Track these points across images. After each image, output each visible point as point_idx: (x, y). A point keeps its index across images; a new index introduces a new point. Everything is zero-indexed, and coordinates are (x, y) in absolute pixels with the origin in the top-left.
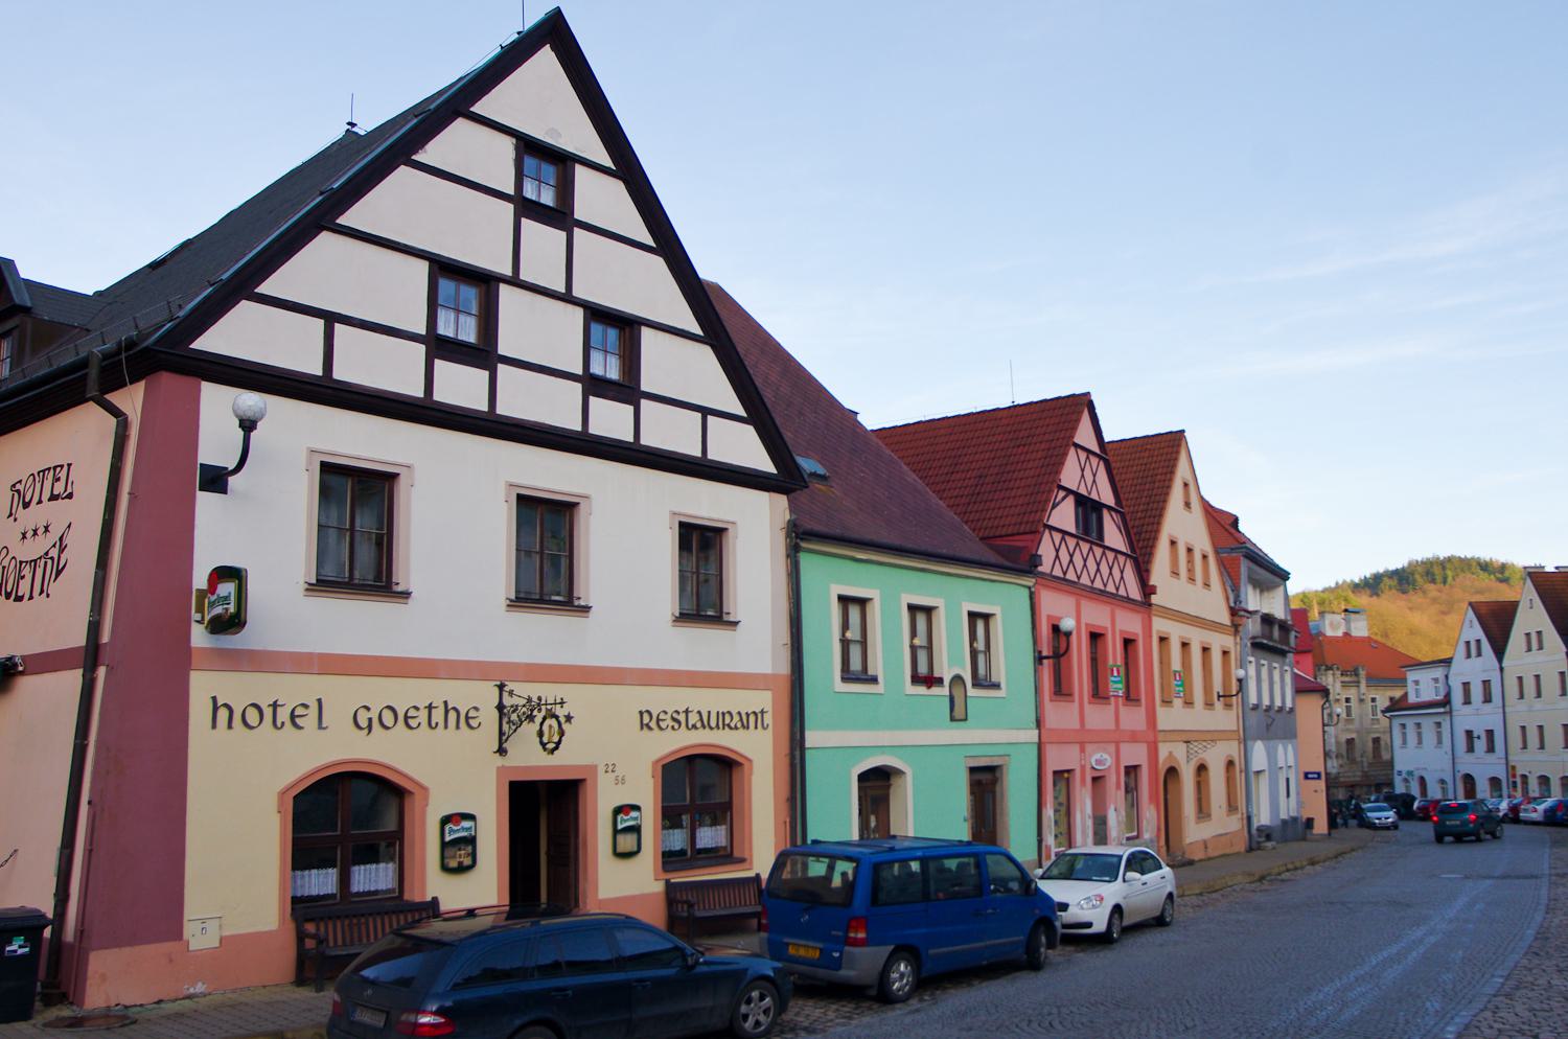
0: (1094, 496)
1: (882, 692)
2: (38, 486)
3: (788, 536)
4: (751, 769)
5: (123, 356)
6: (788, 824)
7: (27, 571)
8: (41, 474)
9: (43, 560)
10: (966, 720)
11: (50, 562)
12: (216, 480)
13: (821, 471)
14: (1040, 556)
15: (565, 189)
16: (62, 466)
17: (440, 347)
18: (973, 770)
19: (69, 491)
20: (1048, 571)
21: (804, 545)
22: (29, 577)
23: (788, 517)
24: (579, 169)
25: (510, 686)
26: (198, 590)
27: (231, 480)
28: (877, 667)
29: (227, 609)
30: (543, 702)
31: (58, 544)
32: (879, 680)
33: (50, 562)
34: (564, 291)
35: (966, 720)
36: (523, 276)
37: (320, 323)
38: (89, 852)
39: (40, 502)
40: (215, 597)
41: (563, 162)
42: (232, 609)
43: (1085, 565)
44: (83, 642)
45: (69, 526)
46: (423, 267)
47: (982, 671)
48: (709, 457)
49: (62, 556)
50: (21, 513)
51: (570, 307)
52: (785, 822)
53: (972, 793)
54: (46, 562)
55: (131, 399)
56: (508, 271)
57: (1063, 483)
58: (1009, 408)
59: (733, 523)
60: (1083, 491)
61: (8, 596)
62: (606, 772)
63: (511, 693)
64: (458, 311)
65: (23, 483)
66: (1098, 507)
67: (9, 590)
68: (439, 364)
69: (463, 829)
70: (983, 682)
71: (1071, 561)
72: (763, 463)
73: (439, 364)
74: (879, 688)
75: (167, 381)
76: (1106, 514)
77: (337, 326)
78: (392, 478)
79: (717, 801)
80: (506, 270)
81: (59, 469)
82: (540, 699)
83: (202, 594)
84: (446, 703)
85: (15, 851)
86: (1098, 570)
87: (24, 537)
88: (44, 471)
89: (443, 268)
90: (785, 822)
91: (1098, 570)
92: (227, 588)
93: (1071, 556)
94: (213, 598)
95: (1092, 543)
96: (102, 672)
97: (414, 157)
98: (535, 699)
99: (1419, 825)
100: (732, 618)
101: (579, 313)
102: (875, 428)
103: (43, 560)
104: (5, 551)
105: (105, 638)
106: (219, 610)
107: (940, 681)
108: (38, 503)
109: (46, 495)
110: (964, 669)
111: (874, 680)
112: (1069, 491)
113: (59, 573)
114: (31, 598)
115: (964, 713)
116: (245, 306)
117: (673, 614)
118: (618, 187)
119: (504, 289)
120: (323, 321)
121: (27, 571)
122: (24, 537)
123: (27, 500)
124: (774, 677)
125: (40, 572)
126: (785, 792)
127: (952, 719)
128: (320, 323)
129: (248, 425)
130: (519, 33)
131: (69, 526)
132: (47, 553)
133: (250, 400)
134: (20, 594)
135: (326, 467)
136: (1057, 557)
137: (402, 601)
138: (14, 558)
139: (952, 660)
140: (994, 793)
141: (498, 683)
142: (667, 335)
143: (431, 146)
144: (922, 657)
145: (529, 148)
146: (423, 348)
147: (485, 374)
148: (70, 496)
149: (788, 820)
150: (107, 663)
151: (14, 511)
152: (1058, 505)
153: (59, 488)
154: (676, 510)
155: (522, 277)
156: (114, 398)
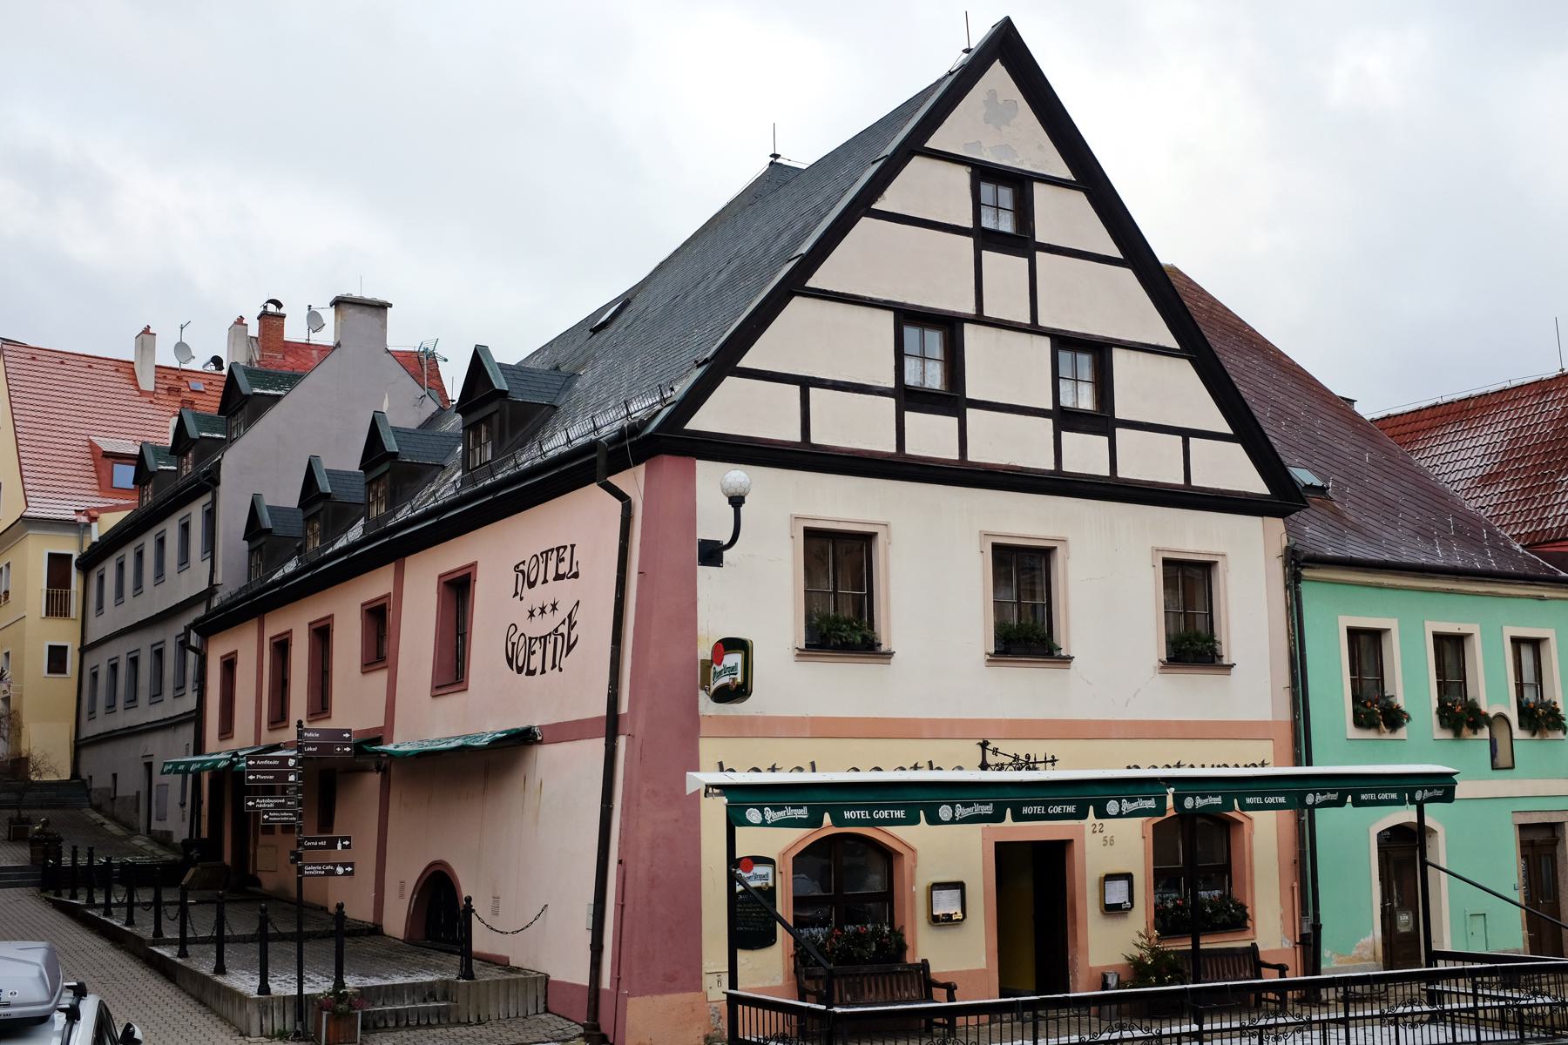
1: (1405, 738)
2: (542, 566)
3: (1286, 564)
4: (1252, 828)
5: (627, 442)
6: (1296, 889)
7: (537, 647)
8: (544, 555)
9: (553, 637)
10: (1512, 767)
11: (560, 638)
12: (712, 554)
13: (1318, 483)
15: (1024, 211)
16: (565, 547)
17: (909, 398)
18: (1523, 828)
19: (574, 570)
21: (1305, 573)
22: (539, 653)
23: (1285, 543)
25: (993, 745)
26: (702, 660)
29: (734, 679)
30: (1032, 760)
31: (567, 621)
33: (560, 638)
34: (1028, 322)
35: (1512, 767)
36: (988, 312)
37: (796, 389)
38: (621, 906)
41: (1020, 183)
42: (739, 678)
44: (604, 713)
45: (577, 604)
46: (888, 318)
48: (1193, 484)
49: (572, 632)
50: (526, 591)
51: (1036, 338)
54: (556, 639)
55: (632, 481)
58: (1557, 378)
61: (520, 670)
62: (1094, 832)
63: (995, 751)
64: (924, 358)
65: (527, 564)
67: (520, 665)
72: (1251, 482)
75: (668, 465)
77: (813, 391)
78: (866, 539)
79: (45, 779)
80: (969, 308)
81: (562, 550)
82: (1028, 757)
83: (706, 665)
84: (930, 763)
85: (546, 906)
87: (532, 614)
88: (547, 552)
89: (907, 316)
90: (1293, 888)
92: (734, 659)
94: (719, 669)
96: (622, 741)
97: (874, 207)
98: (1023, 757)
99: (1374, 935)
100: (884, 648)
101: (1045, 343)
102: (1377, 416)
103: (553, 637)
104: (513, 628)
105: (624, 708)
106: (725, 680)
109: (551, 574)
110: (1509, 708)
113: (570, 648)
114: (543, 672)
116: (730, 382)
117: (1160, 660)
118: (1079, 200)
120: (798, 387)
121: (537, 647)
123: (532, 579)
124: (1275, 723)
125: (550, 648)
127: (1494, 767)
128: (796, 389)
129: (737, 501)
130: (967, 51)
131: (577, 604)
132: (556, 630)
133: (738, 475)
134: (532, 668)
137: (885, 661)
138: (523, 634)
140: (1553, 858)
141: (981, 741)
142: (1141, 354)
143: (889, 192)
145: (983, 173)
146: (892, 401)
147: (1025, 262)
148: (576, 575)
149: (1295, 884)
150: (628, 732)
151: (519, 591)
154: (1160, 545)
155: (1180, 438)
156: (618, 480)
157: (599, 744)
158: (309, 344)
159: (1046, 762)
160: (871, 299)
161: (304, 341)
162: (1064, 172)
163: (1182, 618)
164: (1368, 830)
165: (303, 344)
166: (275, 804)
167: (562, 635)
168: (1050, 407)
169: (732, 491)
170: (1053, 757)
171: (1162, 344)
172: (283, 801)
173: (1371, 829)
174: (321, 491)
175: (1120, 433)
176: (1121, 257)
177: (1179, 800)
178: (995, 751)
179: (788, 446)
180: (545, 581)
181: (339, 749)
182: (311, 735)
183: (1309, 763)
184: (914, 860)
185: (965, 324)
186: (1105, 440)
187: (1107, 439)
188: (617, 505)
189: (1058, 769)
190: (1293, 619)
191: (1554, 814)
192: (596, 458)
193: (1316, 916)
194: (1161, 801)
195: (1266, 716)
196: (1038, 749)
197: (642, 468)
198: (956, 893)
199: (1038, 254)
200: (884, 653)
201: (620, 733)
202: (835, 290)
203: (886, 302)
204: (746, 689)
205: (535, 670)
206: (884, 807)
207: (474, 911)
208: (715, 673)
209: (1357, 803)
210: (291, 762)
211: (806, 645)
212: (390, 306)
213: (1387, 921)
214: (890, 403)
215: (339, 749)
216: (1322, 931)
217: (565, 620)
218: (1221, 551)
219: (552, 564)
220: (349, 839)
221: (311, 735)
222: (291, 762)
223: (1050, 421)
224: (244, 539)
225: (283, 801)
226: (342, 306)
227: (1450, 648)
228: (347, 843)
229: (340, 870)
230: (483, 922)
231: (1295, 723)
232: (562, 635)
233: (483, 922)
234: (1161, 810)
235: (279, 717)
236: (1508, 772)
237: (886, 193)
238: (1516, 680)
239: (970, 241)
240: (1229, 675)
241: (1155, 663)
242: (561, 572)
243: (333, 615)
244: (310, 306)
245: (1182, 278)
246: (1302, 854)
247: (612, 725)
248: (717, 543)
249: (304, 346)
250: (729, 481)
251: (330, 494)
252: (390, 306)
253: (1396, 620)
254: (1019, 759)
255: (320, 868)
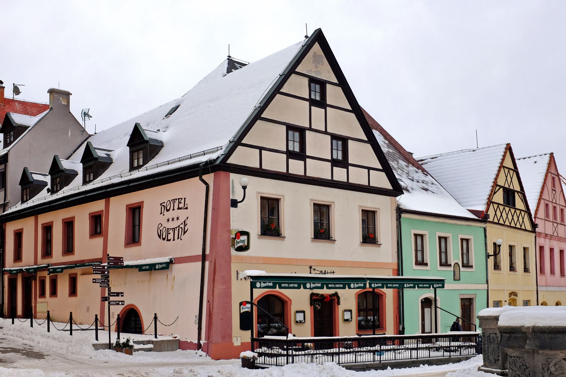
0: (511, 187)
2: (172, 205)
3: (397, 212)
5: (209, 166)
7: (171, 231)
8: (173, 201)
9: (177, 229)
11: (180, 229)
12: (234, 203)
14: (489, 215)
16: (182, 199)
18: (462, 299)
19: (186, 206)
20: (492, 221)
24: (328, 85)
27: (239, 204)
28: (428, 259)
31: (183, 223)
32: (473, 267)
33: (180, 229)
34: (324, 130)
35: (460, 280)
39: (174, 209)
40: (239, 240)
41: (322, 84)
42: (246, 244)
43: (507, 217)
44: (201, 253)
45: (188, 218)
46: (284, 128)
47: (465, 262)
51: (327, 136)
52: (397, 316)
53: (462, 309)
54: (179, 229)
55: (209, 178)
56: (308, 126)
57: (498, 184)
59: (379, 209)
60: (507, 186)
61: (164, 239)
63: (314, 270)
65: (166, 203)
66: (513, 192)
67: (164, 237)
68: (290, 160)
69: (247, 307)
70: (467, 265)
71: (501, 215)
73: (290, 160)
74: (428, 268)
75: (222, 174)
76: (516, 194)
77: (371, 171)
80: (307, 126)
81: (180, 200)
86: (513, 218)
87: (168, 220)
88: (174, 200)
89: (290, 128)
90: (397, 316)
91: (513, 218)
92: (244, 238)
93: (501, 214)
94: (238, 241)
95: (510, 207)
96: (207, 263)
97: (280, 91)
98: (323, 271)
101: (329, 138)
103: (177, 229)
104: (160, 225)
105: (208, 252)
106: (241, 244)
107: (450, 265)
108: (173, 210)
109: (176, 207)
111: (472, 267)
112: (501, 187)
113: (185, 233)
114: (174, 240)
115: (459, 278)
118: (339, 89)
119: (307, 132)
121: (171, 231)
122: (168, 220)
126: (396, 306)
128: (258, 150)
129: (244, 188)
131: (188, 218)
132: (179, 226)
133: (245, 179)
134: (169, 238)
135: (262, 198)
136: (496, 214)
139: (455, 257)
141: (310, 266)
144: (419, 254)
145: (312, 80)
148: (187, 208)
149: (398, 315)
151: (163, 212)
152: (497, 192)
153: (181, 205)
155: (312, 127)
156: (204, 177)
157: (200, 263)
158: (14, 100)
159: (331, 273)
160: (279, 122)
161: (12, 99)
162: (336, 81)
163: (366, 228)
164: (418, 299)
165: (11, 99)
166: (101, 281)
167: (182, 228)
168: (330, 159)
169: (244, 185)
170: (333, 271)
171: (362, 139)
172: (104, 280)
173: (419, 298)
174: (61, 169)
175: (350, 168)
176: (351, 109)
177: (370, 284)
178: (314, 270)
179: (255, 169)
180: (174, 209)
181: (120, 264)
182: (111, 259)
183: (402, 275)
184: (291, 304)
185: (306, 131)
186: (346, 170)
187: (346, 169)
188: (205, 186)
189: (335, 274)
190: (398, 230)
191: (470, 295)
192: (199, 169)
193: (403, 325)
194: (365, 284)
195: (390, 261)
196: (329, 269)
197: (213, 174)
198: (302, 314)
199: (328, 108)
200: (283, 237)
201: (206, 260)
202: (269, 118)
203: (284, 123)
204: (248, 248)
205: (171, 239)
206: (292, 283)
207: (157, 318)
208: (237, 242)
209: (419, 287)
210: (106, 268)
211: (261, 234)
212: (71, 94)
213: (423, 327)
214: (285, 156)
215: (120, 264)
216: (405, 329)
217: (182, 223)
218: (378, 207)
219: (176, 204)
220: (123, 293)
221: (111, 259)
222: (106, 268)
223: (330, 163)
224: (19, 185)
225: (104, 280)
226: (53, 93)
227: (443, 240)
228: (122, 294)
229: (120, 303)
230: (152, 322)
231: (398, 263)
232: (182, 228)
233: (152, 322)
234: (364, 287)
235: (47, 252)
236: (458, 281)
237: (284, 86)
238: (461, 252)
239: (308, 103)
240: (380, 247)
241: (359, 243)
242: (180, 207)
243: (74, 217)
244: (14, 84)
245: (400, 147)
246: (399, 305)
247: (204, 258)
248: (236, 200)
249: (12, 101)
250: (243, 181)
251: (64, 170)
252: (71, 94)
253: (428, 231)
254: (322, 272)
255: (115, 302)
